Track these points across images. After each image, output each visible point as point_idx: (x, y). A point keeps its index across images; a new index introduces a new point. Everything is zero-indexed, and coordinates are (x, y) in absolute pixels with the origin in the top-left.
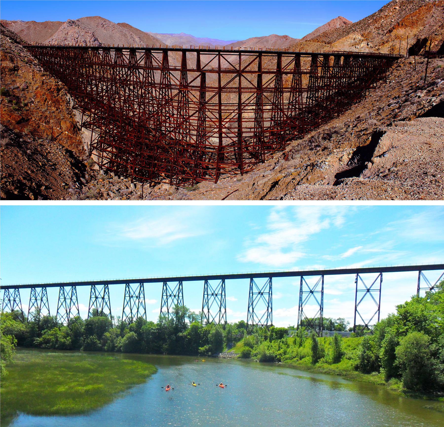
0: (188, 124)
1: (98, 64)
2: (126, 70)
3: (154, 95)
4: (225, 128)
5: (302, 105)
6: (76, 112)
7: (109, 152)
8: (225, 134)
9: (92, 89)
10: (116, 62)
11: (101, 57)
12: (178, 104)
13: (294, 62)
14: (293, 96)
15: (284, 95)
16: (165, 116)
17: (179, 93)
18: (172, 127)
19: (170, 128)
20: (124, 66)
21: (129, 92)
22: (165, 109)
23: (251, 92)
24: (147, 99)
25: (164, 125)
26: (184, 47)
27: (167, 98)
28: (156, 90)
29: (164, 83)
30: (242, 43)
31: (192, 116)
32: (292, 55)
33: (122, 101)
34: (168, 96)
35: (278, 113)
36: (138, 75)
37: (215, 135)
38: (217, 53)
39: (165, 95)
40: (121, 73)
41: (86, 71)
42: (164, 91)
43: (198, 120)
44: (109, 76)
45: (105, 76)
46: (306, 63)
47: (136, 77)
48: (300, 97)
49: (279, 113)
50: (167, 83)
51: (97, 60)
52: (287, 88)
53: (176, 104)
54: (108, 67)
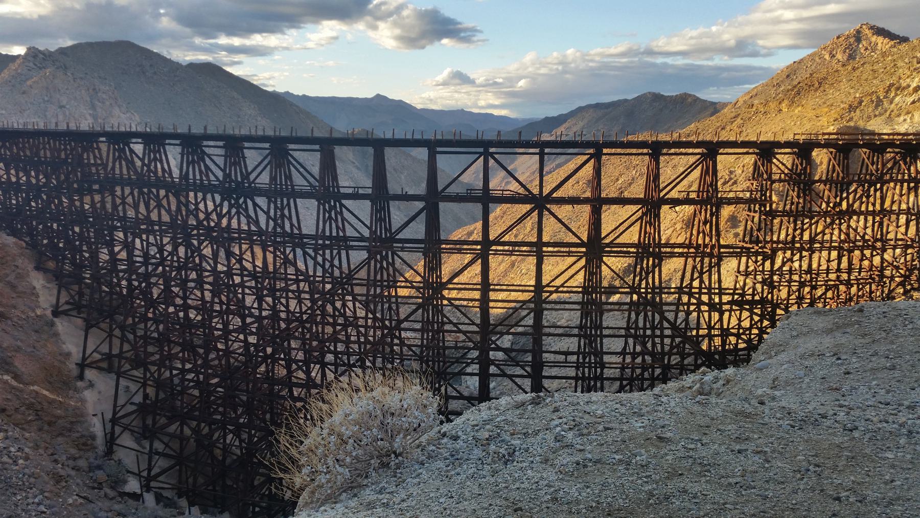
2: (218, 198)
3: (301, 265)
4: (498, 349)
6: (61, 325)
7: (172, 436)
8: (497, 366)
9: (112, 253)
10: (184, 177)
11: (138, 163)
12: (368, 290)
16: (334, 325)
17: (369, 259)
19: (349, 355)
20: (206, 189)
21: (229, 260)
22: (333, 305)
23: (569, 254)
24: (281, 279)
26: (379, 134)
27: (337, 273)
28: (305, 254)
29: (328, 234)
31: (406, 319)
33: (207, 287)
34: (340, 268)
35: (646, 316)
37: (469, 370)
38: (481, 150)
39: (332, 266)
40: (201, 206)
41: (93, 203)
42: (328, 256)
43: (422, 330)
44: (166, 218)
45: (154, 216)
46: (736, 169)
47: (248, 217)
49: (650, 314)
50: (334, 234)
51: (125, 172)
52: (674, 246)
54: (162, 193)
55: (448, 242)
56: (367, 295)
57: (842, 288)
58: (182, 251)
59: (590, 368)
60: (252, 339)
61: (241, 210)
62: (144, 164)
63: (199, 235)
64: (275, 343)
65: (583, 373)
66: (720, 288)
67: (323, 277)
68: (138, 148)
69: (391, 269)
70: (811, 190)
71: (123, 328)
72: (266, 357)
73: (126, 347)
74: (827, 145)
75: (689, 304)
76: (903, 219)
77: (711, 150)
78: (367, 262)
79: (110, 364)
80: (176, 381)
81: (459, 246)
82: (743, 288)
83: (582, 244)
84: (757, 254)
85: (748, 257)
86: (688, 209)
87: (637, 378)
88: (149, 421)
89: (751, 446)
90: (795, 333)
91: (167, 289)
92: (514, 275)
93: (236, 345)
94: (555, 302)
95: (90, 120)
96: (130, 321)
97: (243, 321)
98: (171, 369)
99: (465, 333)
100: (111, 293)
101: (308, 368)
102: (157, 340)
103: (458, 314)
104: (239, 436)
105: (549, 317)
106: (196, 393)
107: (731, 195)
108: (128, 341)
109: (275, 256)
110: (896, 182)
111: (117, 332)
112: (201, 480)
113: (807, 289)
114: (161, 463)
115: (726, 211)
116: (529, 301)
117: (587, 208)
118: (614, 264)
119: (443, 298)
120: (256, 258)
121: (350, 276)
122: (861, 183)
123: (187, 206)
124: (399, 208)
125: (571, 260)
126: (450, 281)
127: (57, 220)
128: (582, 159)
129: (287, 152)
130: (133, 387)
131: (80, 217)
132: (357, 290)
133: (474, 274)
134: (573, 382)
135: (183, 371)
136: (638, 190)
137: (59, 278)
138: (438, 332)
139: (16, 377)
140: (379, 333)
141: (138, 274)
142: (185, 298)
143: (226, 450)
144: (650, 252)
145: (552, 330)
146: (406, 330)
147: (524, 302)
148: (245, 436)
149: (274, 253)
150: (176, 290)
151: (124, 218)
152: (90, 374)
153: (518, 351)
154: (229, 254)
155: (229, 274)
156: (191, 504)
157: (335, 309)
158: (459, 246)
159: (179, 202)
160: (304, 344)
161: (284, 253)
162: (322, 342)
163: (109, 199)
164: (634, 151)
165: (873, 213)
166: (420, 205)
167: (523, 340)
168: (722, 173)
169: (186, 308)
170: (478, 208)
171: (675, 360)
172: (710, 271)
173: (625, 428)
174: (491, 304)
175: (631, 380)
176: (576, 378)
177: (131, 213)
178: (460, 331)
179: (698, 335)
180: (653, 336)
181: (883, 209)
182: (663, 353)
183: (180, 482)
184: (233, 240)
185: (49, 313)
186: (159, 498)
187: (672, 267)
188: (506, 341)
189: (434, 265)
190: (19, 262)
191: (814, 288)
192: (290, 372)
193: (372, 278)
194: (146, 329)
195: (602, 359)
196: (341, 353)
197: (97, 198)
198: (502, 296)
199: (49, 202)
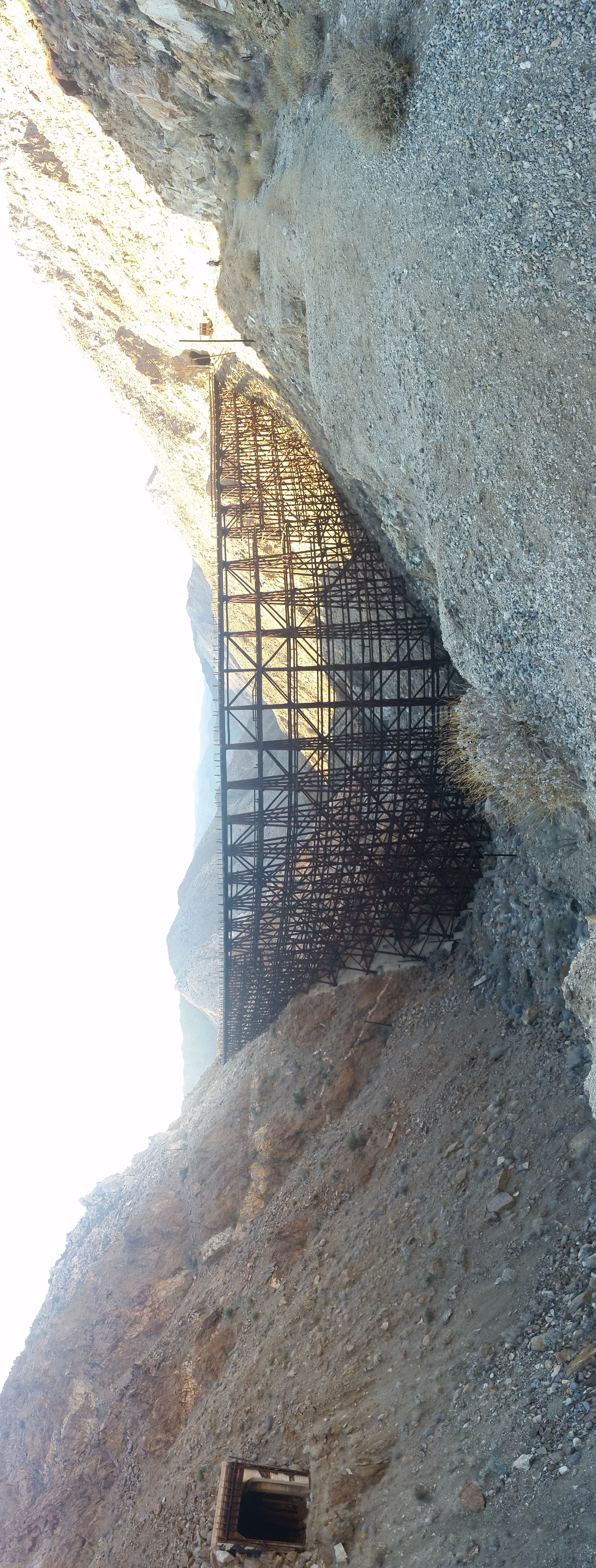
1: (256, 940)
2: (264, 889)
3: (308, 837)
4: (362, 694)
5: (315, 551)
6: (342, 982)
7: (418, 919)
8: (375, 695)
9: (300, 952)
10: (251, 909)
11: (243, 935)
12: (325, 791)
13: (236, 572)
15: (299, 587)
16: (349, 814)
17: (303, 791)
18: (369, 799)
19: (370, 804)
20: (259, 896)
24: (318, 850)
25: (365, 815)
27: (312, 813)
28: (300, 834)
30: (206, 666)
31: (344, 762)
32: (224, 576)
33: (322, 897)
34: (309, 810)
36: (274, 868)
37: (378, 715)
38: (226, 712)
39: (309, 816)
40: (270, 899)
44: (278, 920)
45: (277, 927)
46: (236, 549)
47: (276, 871)
48: (303, 555)
50: (287, 815)
53: (325, 794)
54: (262, 921)
55: (290, 733)
56: (328, 791)
57: (303, 480)
58: (298, 911)
59: (372, 630)
60: (358, 869)
61: (272, 875)
62: (244, 932)
63: (288, 901)
64: (361, 854)
65: (376, 635)
67: (316, 822)
68: (234, 934)
69: (310, 775)
70: (246, 504)
71: (347, 948)
73: (358, 946)
74: (219, 498)
75: (323, 569)
76: (260, 453)
77: (224, 566)
78: (306, 792)
79: (369, 956)
80: (383, 916)
81: (292, 726)
83: (288, 641)
84: (287, 531)
85: (290, 536)
87: (376, 598)
88: (407, 934)
90: (355, 462)
91: (323, 920)
92: (312, 685)
93: (361, 879)
95: (218, 960)
96: (342, 943)
97: (346, 874)
98: (374, 919)
99: (352, 718)
100: (324, 954)
102: (355, 927)
103: (338, 725)
104: (423, 878)
105: (338, 661)
106: (391, 904)
107: (251, 552)
108: (355, 945)
109: (303, 854)
110: (239, 459)
111: (349, 951)
112: (450, 902)
113: (307, 500)
114: (436, 928)
115: (261, 553)
116: (328, 674)
117: (264, 639)
119: (329, 736)
120: (304, 865)
121: (315, 803)
122: (240, 478)
123: (270, 908)
126: (316, 731)
127: (279, 980)
128: (232, 647)
129: (233, 846)
130: (384, 943)
131: (277, 968)
132: (325, 799)
133: (311, 714)
134: (383, 641)
135: (377, 912)
137: (314, 982)
138: (353, 738)
141: (314, 938)
142: (329, 910)
143: (430, 886)
144: (290, 596)
147: (329, 678)
148: (423, 874)
149: (300, 855)
151: (278, 944)
152: (373, 967)
154: (301, 883)
155: (314, 883)
156: (465, 908)
157: (338, 814)
158: (292, 726)
159: (268, 912)
160: (362, 835)
161: (300, 848)
163: (266, 952)
164: (225, 614)
165: (258, 469)
166: (265, 754)
168: (237, 558)
169: (335, 909)
170: (265, 713)
174: (332, 700)
176: (380, 639)
177: (275, 940)
178: (351, 722)
180: (347, 590)
181: (255, 464)
183: (449, 915)
185: (334, 988)
186: (458, 929)
187: (299, 583)
188: (357, 690)
189: (304, 743)
190: (303, 1002)
191: (305, 496)
192: (381, 844)
193: (316, 788)
194: (348, 934)
195: (365, 623)
196: (369, 809)
197: (265, 958)
199: (267, 984)
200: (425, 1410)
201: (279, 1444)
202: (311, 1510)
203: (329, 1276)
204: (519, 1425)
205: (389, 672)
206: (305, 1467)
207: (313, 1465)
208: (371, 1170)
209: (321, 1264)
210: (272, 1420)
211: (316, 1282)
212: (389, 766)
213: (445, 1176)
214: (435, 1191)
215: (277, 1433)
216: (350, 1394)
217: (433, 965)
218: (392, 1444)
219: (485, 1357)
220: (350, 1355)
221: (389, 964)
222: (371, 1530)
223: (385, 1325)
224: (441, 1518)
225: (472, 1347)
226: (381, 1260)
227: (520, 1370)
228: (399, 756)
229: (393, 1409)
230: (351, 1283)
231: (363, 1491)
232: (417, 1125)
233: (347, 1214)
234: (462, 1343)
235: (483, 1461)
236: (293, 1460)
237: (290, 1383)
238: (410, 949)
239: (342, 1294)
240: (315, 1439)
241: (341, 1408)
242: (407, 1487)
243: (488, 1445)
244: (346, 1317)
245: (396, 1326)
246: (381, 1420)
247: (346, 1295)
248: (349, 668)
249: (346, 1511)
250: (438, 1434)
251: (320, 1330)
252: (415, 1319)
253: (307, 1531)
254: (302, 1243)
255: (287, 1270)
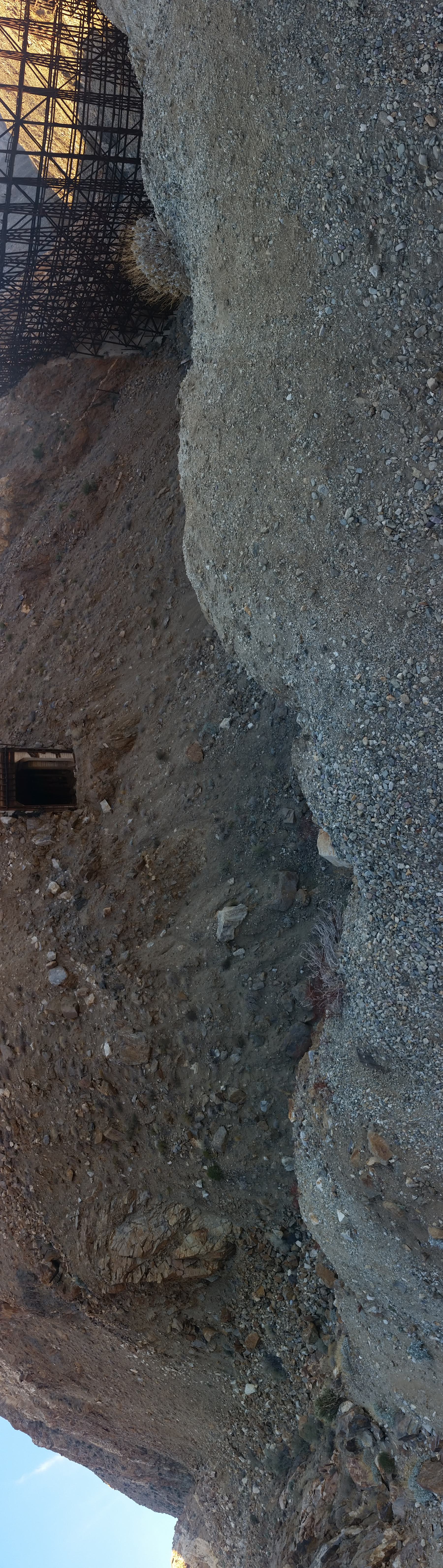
0: (100, 205)
4: (109, 151)
9: (35, 338)
14: (66, 39)
16: (87, 237)
23: (53, 107)
27: (55, 234)
28: (41, 250)
31: (87, 199)
34: (51, 232)
35: (94, 69)
39: (50, 236)
42: (44, 238)
45: (14, 318)
52: (53, 47)
56: (70, 219)
60: (91, 279)
63: (25, 300)
66: (80, 27)
72: (102, 273)
73: (89, 336)
78: (49, 218)
79: (97, 344)
80: (110, 315)
82: (81, 15)
86: (31, 38)
88: (129, 329)
89: (177, 58)
92: (65, 139)
94: (83, 117)
97: (80, 283)
98: (103, 317)
99: (98, 169)
101: (111, 253)
105: (92, 122)
106: (117, 307)
107: (23, 11)
109: (42, 265)
111: (80, 340)
114: (151, 326)
115: (33, 16)
116: (81, 133)
117: (24, 94)
118: (61, 82)
119: (75, 178)
120: (42, 274)
124: (16, 198)
125: (57, 106)
126: (65, 174)
130: (111, 335)
133: (62, 162)
135: (105, 312)
136: (16, 64)
139: (102, 379)
140: (94, 214)
144: (54, 61)
145: (100, 120)
146: (94, 199)
147: (82, 136)
149: (40, 266)
150: (58, 313)
151: (15, 332)
152: (101, 353)
153: (111, 140)
154: (38, 287)
158: (43, 167)
160: (97, 254)
162: (96, 244)
166: (13, 187)
167: (104, 136)
169: (69, 309)
170: (18, 157)
171: (120, 57)
172: (69, 31)
173: (164, 122)
174: (82, 153)
175: (130, 82)
176: (128, 110)
178: (97, 172)
179: (106, 43)
182: (116, 63)
184: (30, 285)
187: (65, 51)
188: (105, 146)
189: (55, 182)
194: (80, 326)
198: (77, 146)
200: (158, 695)
201: (43, 730)
202: (78, 778)
203: (73, 599)
204: (221, 698)
205: (133, 136)
206: (69, 746)
207: (75, 744)
208: (103, 509)
209: (66, 589)
210: (34, 715)
211: (63, 605)
212: (124, 205)
213: (158, 513)
214: (151, 525)
215: (40, 723)
216: (100, 689)
217: (148, 354)
218: (137, 721)
219: (195, 650)
220: (96, 660)
221: (113, 351)
222: (127, 788)
223: (122, 633)
224: (176, 771)
225: (185, 644)
226: (116, 582)
227: (218, 657)
228: (132, 199)
229: (135, 697)
230: (93, 603)
231: (118, 759)
232: (137, 474)
233: (84, 548)
234: (178, 641)
235: (201, 726)
236: (58, 742)
237: (47, 685)
238: (131, 340)
239: (85, 613)
240: (75, 724)
241: (94, 700)
242: (151, 752)
243: (202, 715)
244: (90, 630)
245: (130, 633)
246: (127, 706)
247: (89, 613)
248: (99, 129)
249: (107, 776)
250: (169, 711)
251: (69, 643)
252: (144, 627)
253: (77, 795)
254: (47, 573)
255: (36, 596)
